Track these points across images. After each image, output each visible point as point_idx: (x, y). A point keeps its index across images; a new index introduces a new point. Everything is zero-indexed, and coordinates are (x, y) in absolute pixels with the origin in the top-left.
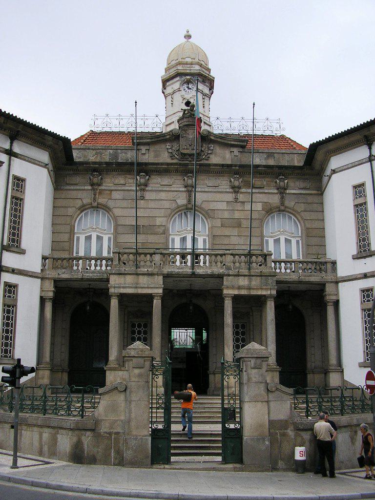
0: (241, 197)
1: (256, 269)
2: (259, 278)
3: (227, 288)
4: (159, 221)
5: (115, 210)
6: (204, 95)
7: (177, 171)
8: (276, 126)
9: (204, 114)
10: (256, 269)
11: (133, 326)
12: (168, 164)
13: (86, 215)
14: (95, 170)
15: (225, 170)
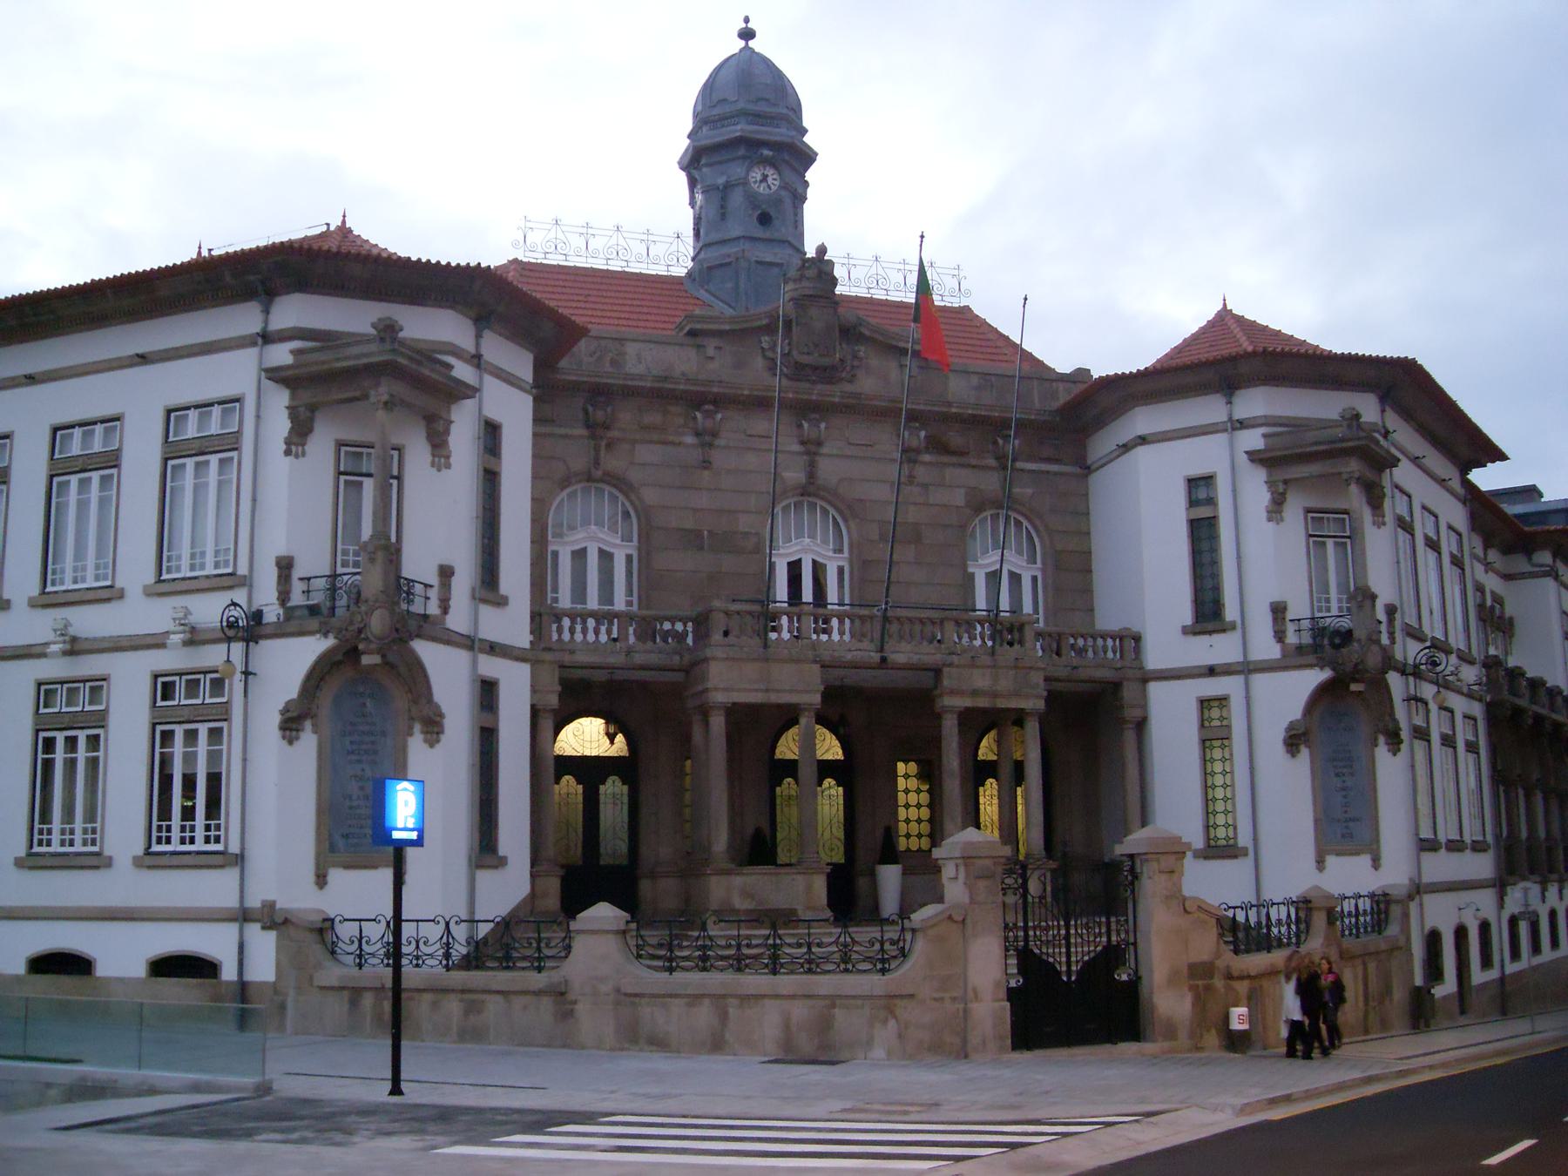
0: (920, 471)
3: (952, 692)
13: (572, 496)
15: (883, 413)
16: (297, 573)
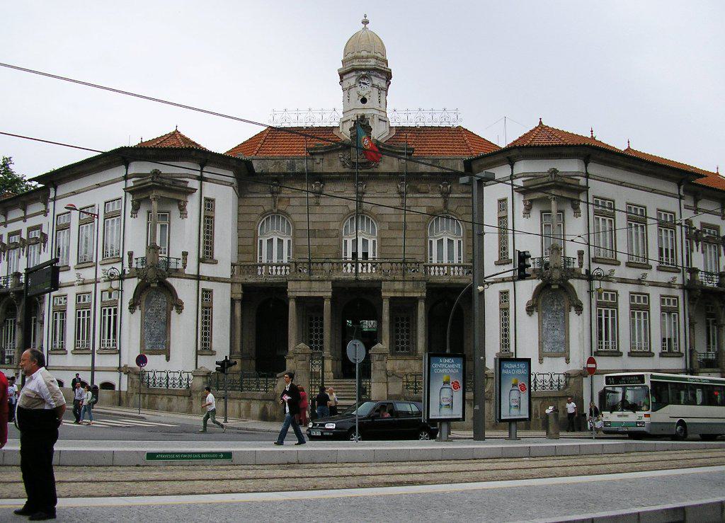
1: (410, 275)
2: (412, 283)
3: (385, 291)
4: (332, 226)
5: (293, 216)
6: (380, 89)
7: (349, 179)
8: (453, 117)
9: (380, 109)
10: (410, 275)
11: (311, 319)
12: (339, 173)
14: (276, 179)
15: (391, 177)
16: (134, 257)
